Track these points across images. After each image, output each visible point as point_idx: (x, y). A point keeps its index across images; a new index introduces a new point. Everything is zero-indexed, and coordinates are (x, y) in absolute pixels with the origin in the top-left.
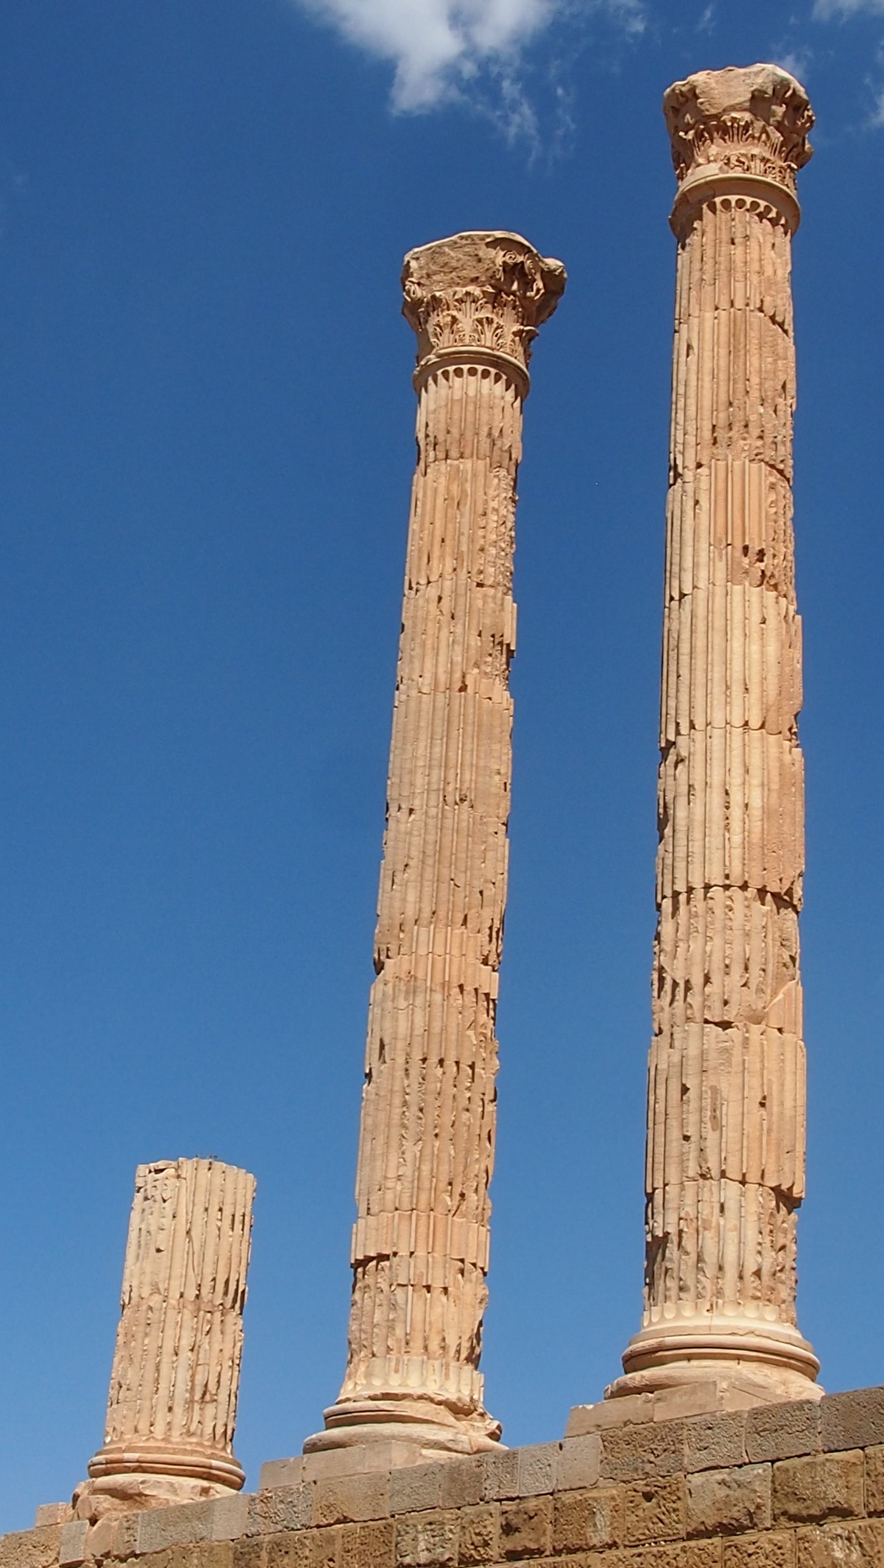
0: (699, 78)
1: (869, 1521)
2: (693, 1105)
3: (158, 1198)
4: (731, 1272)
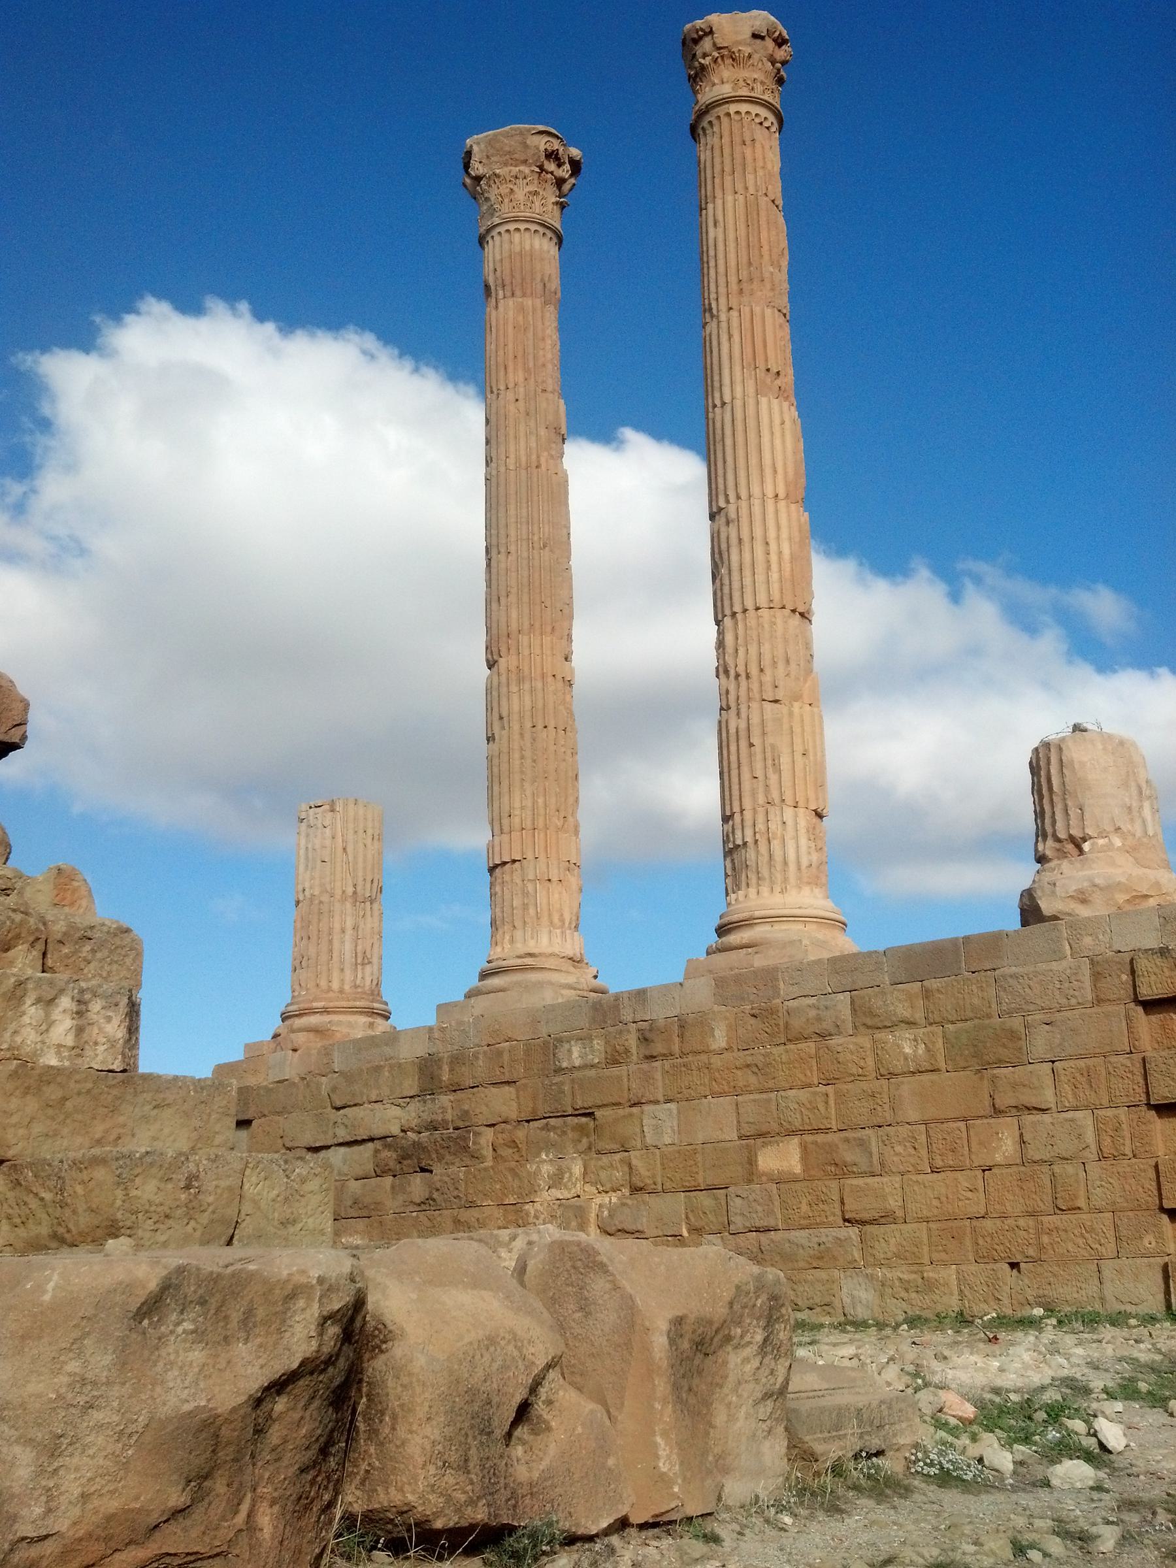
0: (714, 19)
1: (929, 1028)
2: (759, 757)
3: (320, 825)
4: (792, 867)
